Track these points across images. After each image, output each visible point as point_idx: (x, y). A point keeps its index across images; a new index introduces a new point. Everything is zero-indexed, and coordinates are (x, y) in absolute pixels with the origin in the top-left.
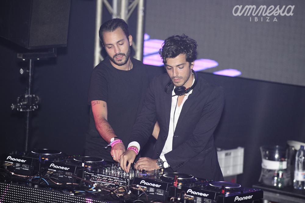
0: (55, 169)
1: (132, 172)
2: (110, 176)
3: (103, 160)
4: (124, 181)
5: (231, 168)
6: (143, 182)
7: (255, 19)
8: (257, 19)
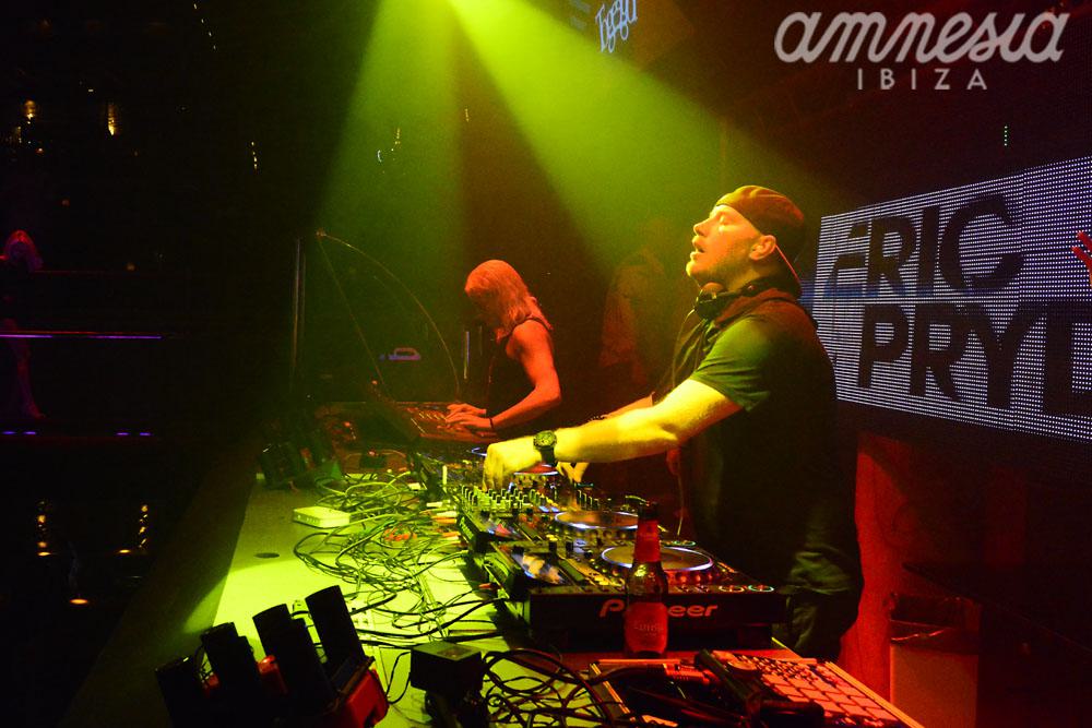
7: (883, 78)
8: (889, 77)
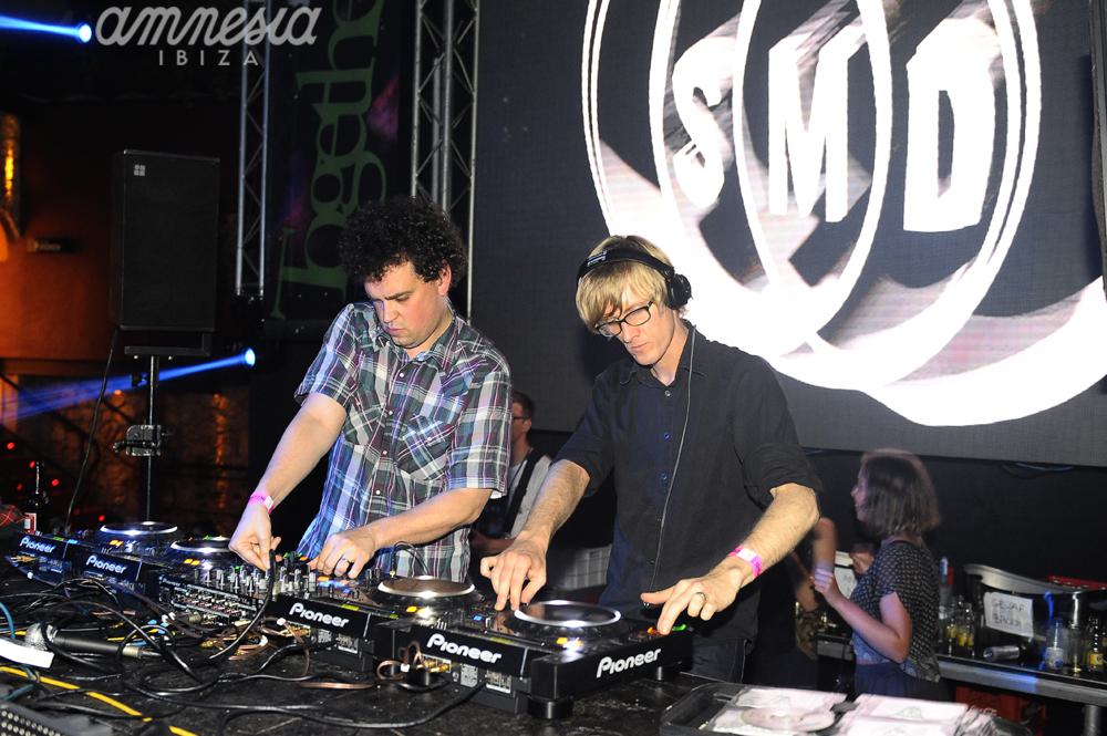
0: (446, 654)
1: (194, 558)
2: (210, 588)
3: (618, 615)
4: (251, 605)
5: (587, 577)
6: (436, 640)
